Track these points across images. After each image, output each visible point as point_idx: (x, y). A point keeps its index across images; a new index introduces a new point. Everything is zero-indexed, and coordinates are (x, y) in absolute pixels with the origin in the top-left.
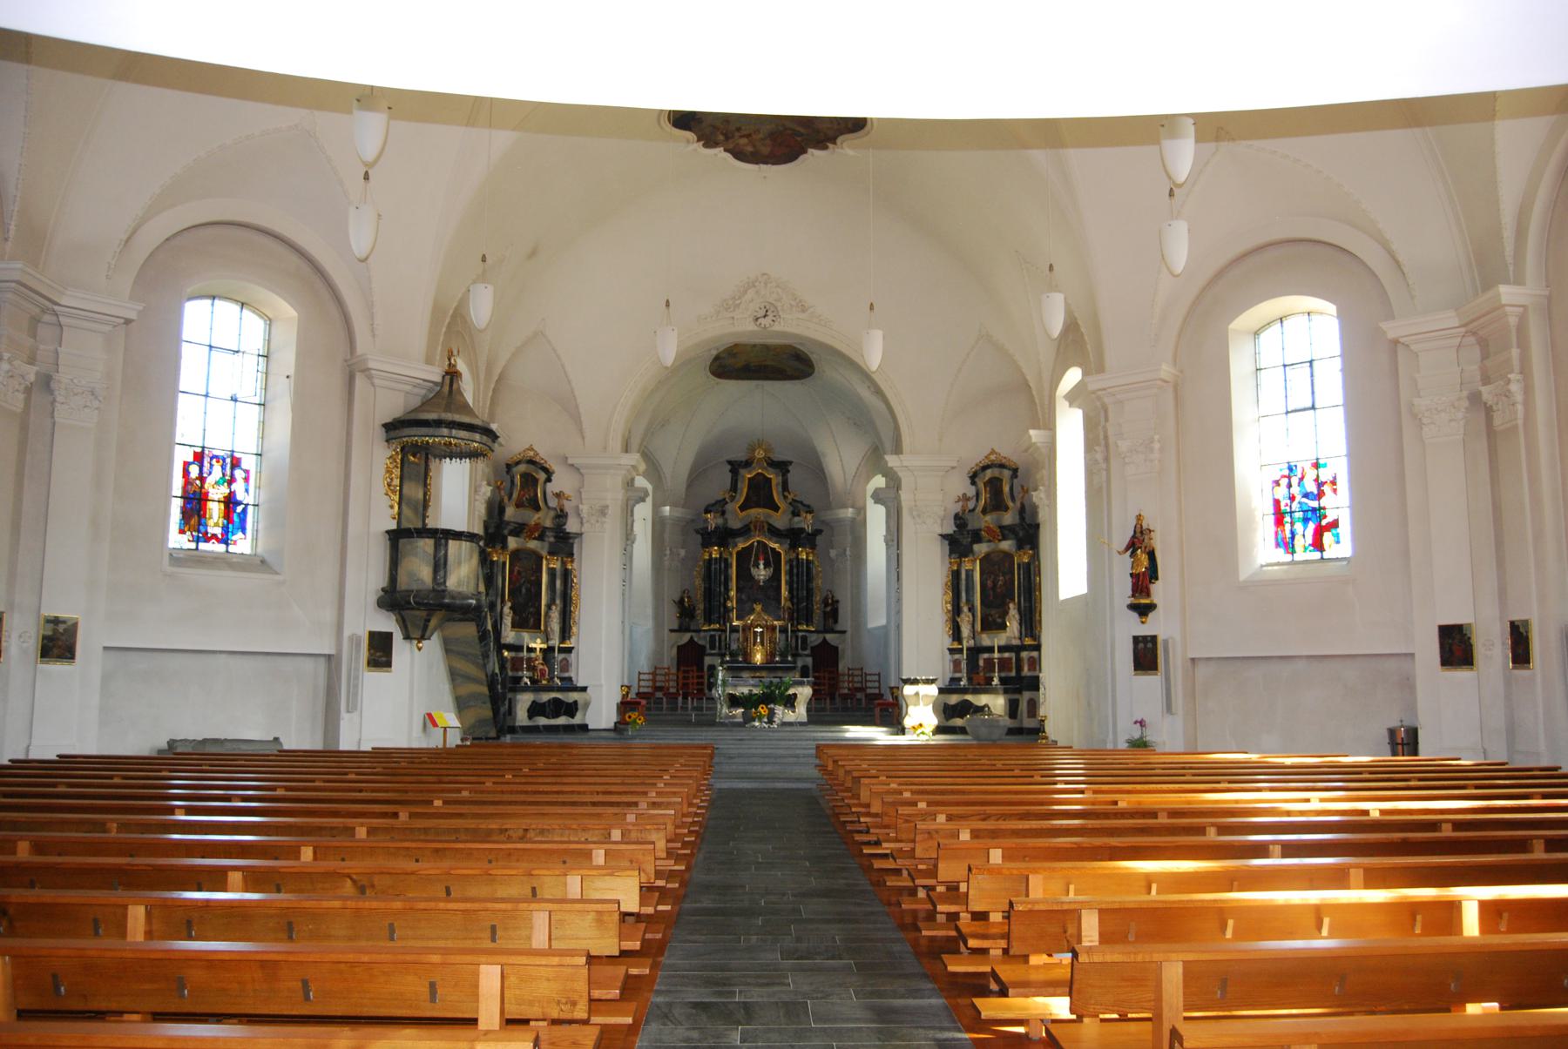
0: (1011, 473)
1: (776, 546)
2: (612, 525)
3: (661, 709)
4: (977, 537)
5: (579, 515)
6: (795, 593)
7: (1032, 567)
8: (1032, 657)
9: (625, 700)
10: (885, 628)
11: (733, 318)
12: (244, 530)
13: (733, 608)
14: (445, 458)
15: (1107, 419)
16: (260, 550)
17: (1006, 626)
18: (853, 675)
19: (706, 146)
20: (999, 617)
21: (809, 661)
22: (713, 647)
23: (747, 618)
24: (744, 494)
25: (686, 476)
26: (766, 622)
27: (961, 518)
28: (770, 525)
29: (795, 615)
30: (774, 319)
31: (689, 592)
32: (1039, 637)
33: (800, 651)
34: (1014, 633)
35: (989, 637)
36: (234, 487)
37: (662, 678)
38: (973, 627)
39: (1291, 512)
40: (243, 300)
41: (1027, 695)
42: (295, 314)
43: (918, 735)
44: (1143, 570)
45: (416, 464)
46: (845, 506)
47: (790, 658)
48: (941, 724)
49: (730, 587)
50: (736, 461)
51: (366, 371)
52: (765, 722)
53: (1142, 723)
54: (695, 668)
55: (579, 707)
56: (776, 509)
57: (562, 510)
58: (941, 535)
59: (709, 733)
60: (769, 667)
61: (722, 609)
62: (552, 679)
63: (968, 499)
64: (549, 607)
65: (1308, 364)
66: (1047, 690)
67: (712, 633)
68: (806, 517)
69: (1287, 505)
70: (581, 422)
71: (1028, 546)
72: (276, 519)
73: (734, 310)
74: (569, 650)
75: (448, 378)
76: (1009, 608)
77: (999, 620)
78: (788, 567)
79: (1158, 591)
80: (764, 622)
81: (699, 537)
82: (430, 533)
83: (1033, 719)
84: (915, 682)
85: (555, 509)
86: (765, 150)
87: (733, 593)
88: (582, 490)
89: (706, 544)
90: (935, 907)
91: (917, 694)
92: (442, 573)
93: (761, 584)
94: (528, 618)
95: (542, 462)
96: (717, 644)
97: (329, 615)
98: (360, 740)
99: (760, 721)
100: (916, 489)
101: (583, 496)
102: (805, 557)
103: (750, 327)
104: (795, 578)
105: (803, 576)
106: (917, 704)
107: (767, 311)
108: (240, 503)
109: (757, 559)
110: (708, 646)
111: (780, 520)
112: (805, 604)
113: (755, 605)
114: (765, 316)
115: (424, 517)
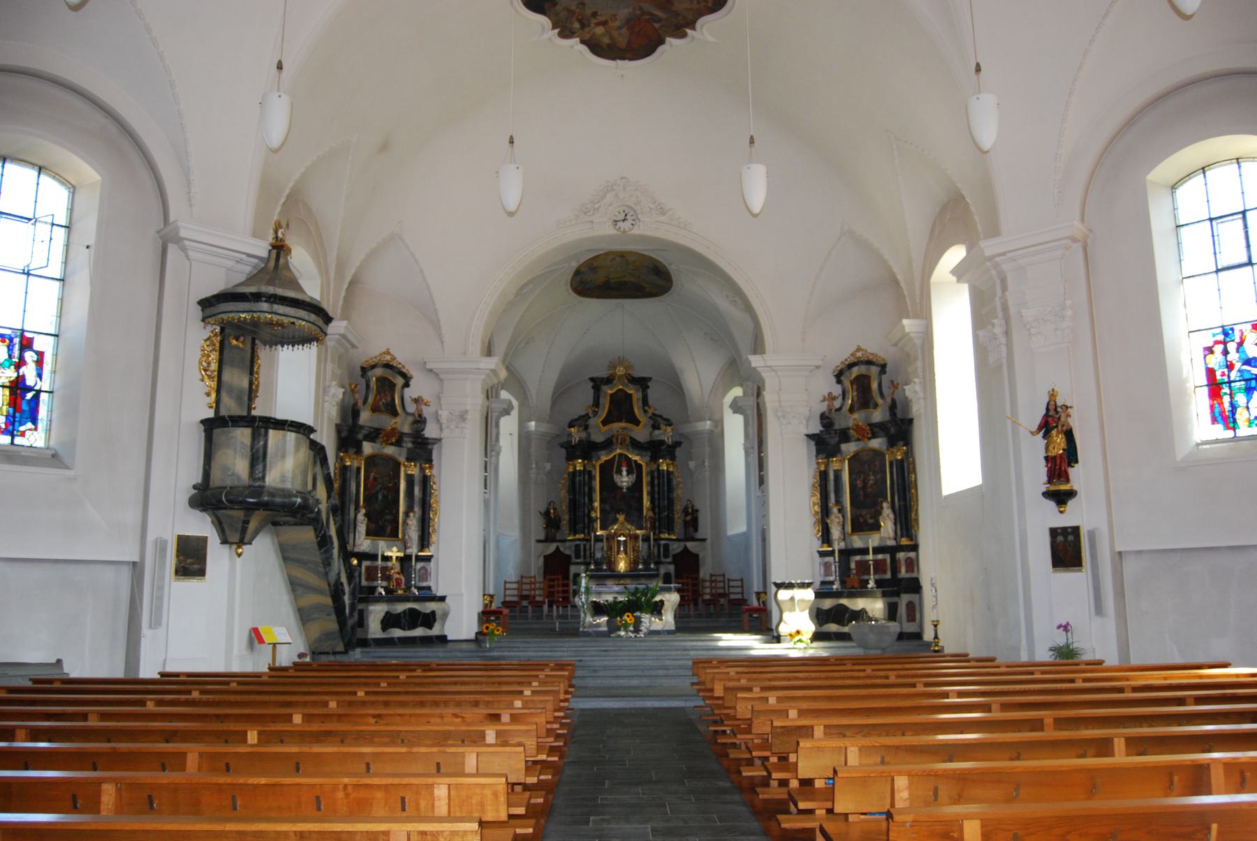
0: (879, 369)
1: (637, 458)
2: (472, 434)
3: (527, 618)
4: (845, 436)
5: (438, 421)
6: (656, 503)
7: (906, 464)
8: (909, 558)
9: (488, 609)
10: (746, 536)
11: (592, 222)
12: (34, 420)
13: (597, 518)
14: (276, 345)
15: (1004, 289)
16: (52, 443)
17: (880, 526)
18: (715, 581)
19: (563, 35)
20: (871, 518)
21: (671, 568)
22: (578, 556)
23: (610, 528)
24: (607, 409)
25: (553, 385)
26: (630, 531)
27: (827, 418)
28: (631, 438)
29: (657, 524)
30: (634, 222)
31: (554, 503)
32: (916, 536)
33: (663, 559)
34: (889, 533)
35: (860, 539)
36: (22, 370)
37: (528, 587)
38: (843, 528)
39: (1230, 382)
40: (41, 164)
41: (905, 599)
42: (98, 178)
43: (795, 643)
44: (1061, 452)
45: (242, 349)
46: (702, 419)
47: (652, 566)
48: (818, 631)
49: (594, 499)
50: (598, 378)
51: (178, 240)
52: (631, 631)
53: (1066, 628)
54: (560, 577)
55: (437, 617)
56: (637, 423)
57: (420, 416)
58: (808, 436)
59: (572, 644)
60: (632, 574)
61: (586, 520)
62: (408, 588)
63: (834, 398)
64: (407, 514)
65: (1241, 216)
66: (938, 591)
67: (578, 543)
68: (665, 430)
69: (1223, 374)
70: (440, 327)
71: (901, 443)
72: (70, 405)
73: (593, 214)
74: (428, 559)
75: (275, 251)
76: (882, 508)
77: (871, 521)
78: (649, 479)
79: (1078, 476)
80: (627, 532)
81: (564, 451)
82: (246, 422)
83: (913, 623)
84: (790, 586)
85: (413, 415)
86: (622, 42)
87: (597, 504)
88: (441, 395)
89: (570, 457)
90: (770, 774)
91: (792, 599)
92: (260, 467)
93: (625, 490)
94: (384, 525)
95: (400, 366)
96: (582, 553)
97: (132, 516)
98: (165, 660)
99: (626, 630)
100: (780, 390)
101: (442, 402)
102: (665, 468)
103: (610, 231)
104: (656, 489)
105: (664, 486)
106: (792, 609)
107: (626, 215)
108: (30, 389)
109: (620, 466)
110: (573, 556)
111: (641, 433)
112: (666, 513)
113: (618, 516)
114: (624, 220)
115: (250, 409)
